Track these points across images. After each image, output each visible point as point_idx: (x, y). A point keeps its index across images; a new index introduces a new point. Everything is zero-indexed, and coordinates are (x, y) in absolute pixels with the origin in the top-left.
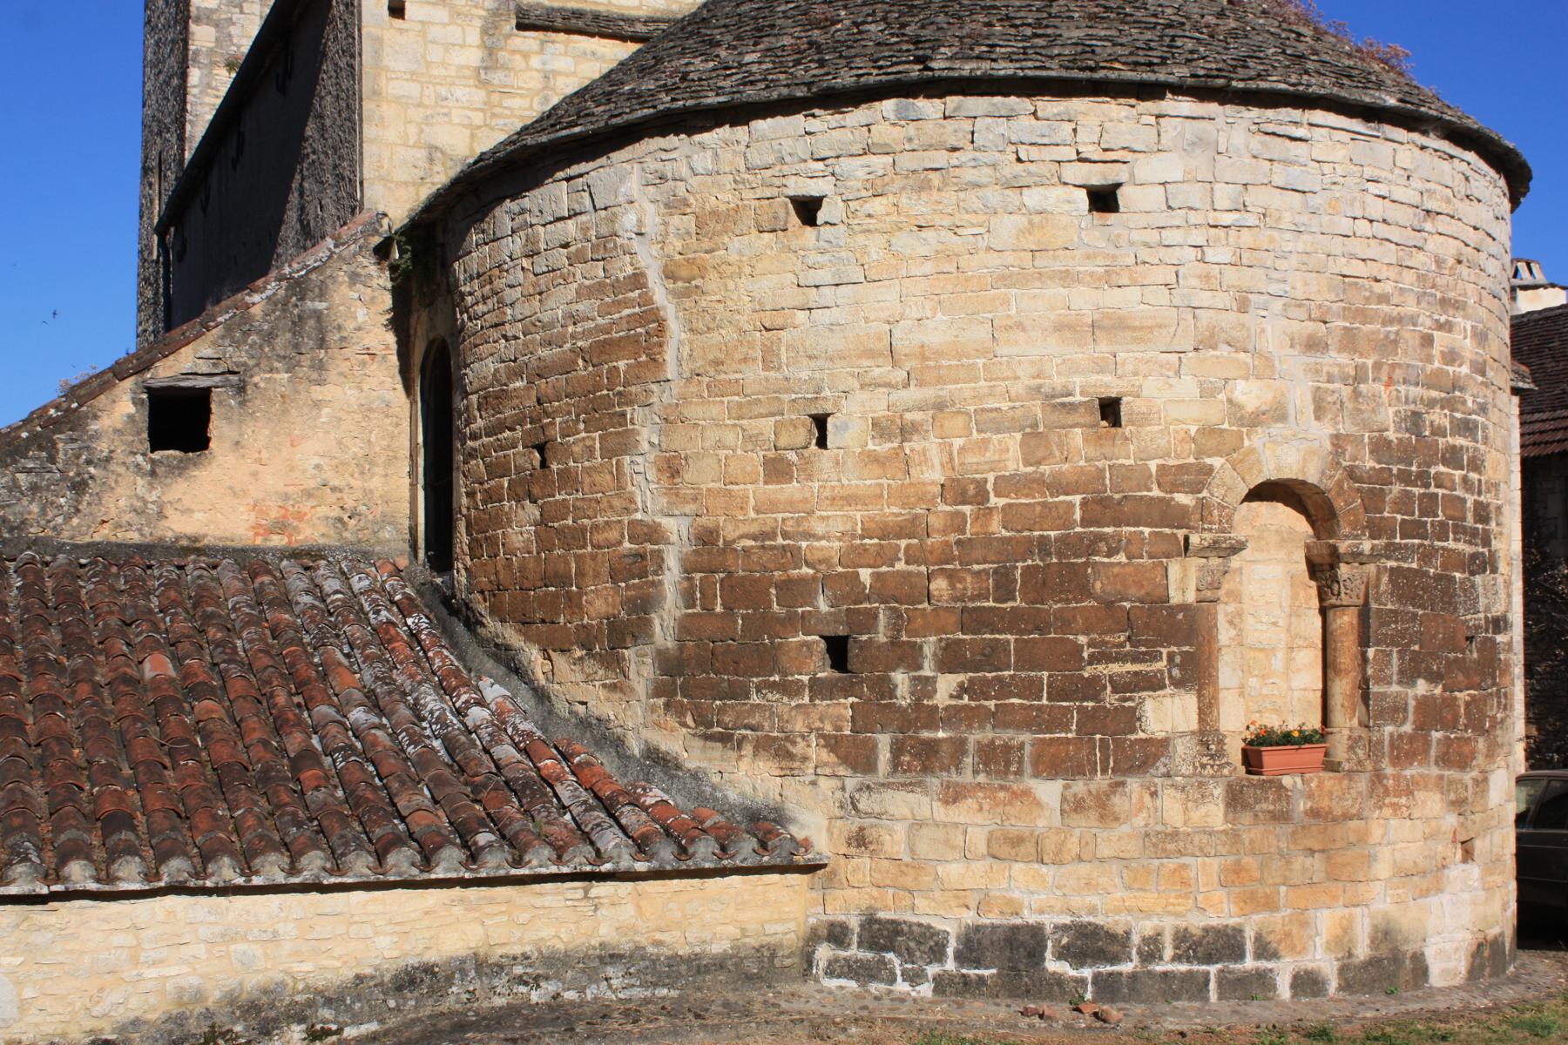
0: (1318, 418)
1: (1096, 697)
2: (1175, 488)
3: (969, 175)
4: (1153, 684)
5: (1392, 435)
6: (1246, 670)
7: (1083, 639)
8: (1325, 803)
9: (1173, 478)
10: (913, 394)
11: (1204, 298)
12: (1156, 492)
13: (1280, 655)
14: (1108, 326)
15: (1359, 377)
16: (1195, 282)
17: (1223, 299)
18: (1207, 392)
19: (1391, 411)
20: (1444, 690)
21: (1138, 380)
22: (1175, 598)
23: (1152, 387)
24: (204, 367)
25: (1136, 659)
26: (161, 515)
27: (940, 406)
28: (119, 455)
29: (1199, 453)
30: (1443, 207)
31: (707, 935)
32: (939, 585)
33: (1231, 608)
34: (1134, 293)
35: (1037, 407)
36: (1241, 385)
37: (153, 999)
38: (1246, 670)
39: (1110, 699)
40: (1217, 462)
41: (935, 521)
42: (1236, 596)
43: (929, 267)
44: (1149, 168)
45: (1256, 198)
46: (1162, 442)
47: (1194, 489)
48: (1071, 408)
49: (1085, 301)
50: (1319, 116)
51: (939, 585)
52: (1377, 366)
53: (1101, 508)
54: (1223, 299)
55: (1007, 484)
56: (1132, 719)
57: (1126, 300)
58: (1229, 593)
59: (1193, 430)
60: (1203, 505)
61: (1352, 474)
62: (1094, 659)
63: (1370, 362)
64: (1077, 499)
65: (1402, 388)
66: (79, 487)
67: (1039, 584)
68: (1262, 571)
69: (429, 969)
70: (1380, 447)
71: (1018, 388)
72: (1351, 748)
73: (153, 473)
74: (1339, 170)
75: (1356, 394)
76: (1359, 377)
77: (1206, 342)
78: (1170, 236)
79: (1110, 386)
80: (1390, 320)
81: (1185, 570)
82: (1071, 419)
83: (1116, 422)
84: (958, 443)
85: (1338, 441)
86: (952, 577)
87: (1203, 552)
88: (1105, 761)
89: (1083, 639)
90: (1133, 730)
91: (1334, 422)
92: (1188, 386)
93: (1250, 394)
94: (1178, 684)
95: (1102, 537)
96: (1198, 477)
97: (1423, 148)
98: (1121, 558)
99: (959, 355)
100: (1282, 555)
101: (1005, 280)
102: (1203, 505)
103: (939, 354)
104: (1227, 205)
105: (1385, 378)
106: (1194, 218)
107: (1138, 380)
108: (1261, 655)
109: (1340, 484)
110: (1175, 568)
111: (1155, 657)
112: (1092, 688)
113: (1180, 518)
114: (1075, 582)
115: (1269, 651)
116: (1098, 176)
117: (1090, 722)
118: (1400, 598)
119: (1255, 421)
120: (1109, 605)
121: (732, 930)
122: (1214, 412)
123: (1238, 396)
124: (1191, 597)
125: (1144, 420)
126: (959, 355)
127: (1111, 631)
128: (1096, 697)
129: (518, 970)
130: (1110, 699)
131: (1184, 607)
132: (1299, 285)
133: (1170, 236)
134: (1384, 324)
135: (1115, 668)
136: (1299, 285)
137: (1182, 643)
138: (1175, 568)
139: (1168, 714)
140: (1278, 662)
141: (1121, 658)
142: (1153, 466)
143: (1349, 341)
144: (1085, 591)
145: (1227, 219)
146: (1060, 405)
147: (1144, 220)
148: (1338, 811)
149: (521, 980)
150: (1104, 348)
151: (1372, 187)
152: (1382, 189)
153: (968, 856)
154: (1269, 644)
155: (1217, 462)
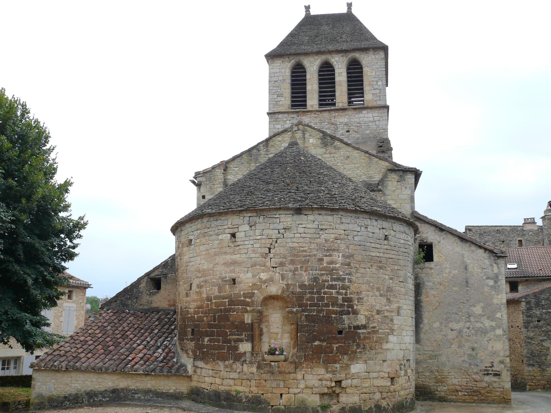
0: (282, 280)
1: (230, 343)
2: (245, 297)
3: (211, 233)
4: (241, 341)
5: (306, 283)
6: (270, 338)
7: (228, 331)
8: (283, 369)
9: (245, 295)
10: (202, 279)
11: (253, 255)
12: (242, 298)
13: (279, 335)
14: (234, 263)
15: (296, 269)
16: (251, 252)
17: (257, 255)
18: (254, 276)
19: (306, 278)
20: (327, 344)
21: (239, 274)
22: (246, 322)
23: (241, 275)
24: (159, 273)
25: (238, 335)
26: (151, 303)
27: (206, 281)
28: (144, 291)
29: (252, 290)
30: (328, 227)
31: (169, 388)
32: (205, 318)
33: (266, 324)
34: (238, 256)
35: (220, 281)
36: (262, 274)
37: (73, 390)
38: (270, 338)
39: (233, 343)
40: (256, 291)
41: (205, 305)
42: (268, 321)
43: (204, 253)
44: (242, 228)
45: (265, 232)
46: (244, 288)
47: (251, 298)
48: (226, 281)
49: (228, 258)
50: (281, 212)
51: (205, 318)
52: (301, 267)
53: (231, 303)
54: (257, 255)
55: (216, 297)
56: (237, 348)
57: (237, 257)
58: (266, 321)
59: (251, 285)
60: (252, 301)
61: (292, 293)
62: (230, 335)
63: (299, 266)
64: (227, 300)
65: (311, 272)
66: (137, 298)
67: (221, 318)
68: (274, 315)
69: (118, 390)
70: (302, 286)
71: (217, 277)
72: (292, 357)
73: (150, 295)
74: (289, 223)
75: (294, 274)
76: (296, 269)
77: (254, 265)
78: (246, 243)
79: (234, 275)
80: (306, 256)
81: (248, 316)
82: (226, 283)
83: (234, 283)
84: (208, 289)
85: (287, 285)
86: (207, 317)
87: (251, 312)
88: (232, 357)
89: (228, 331)
90: (237, 351)
91: (287, 281)
92: (250, 275)
93: (264, 276)
94: (247, 341)
95: (231, 308)
96: (252, 295)
97: (320, 214)
98: (235, 313)
99: (208, 271)
100: (280, 312)
101: (215, 255)
102: (252, 301)
103: (206, 271)
104: (258, 234)
105: (304, 270)
106: (251, 238)
107: (239, 274)
108: (274, 335)
109: (288, 295)
110: (246, 315)
111: (242, 335)
112: (229, 341)
113: (248, 304)
114: (227, 318)
115: (277, 334)
116: (232, 231)
117: (229, 348)
118: (308, 322)
119: (265, 282)
120: (233, 323)
121: (174, 388)
122: (255, 280)
123: (261, 277)
124: (250, 322)
125: (240, 283)
126: (208, 271)
127: (233, 329)
128: (230, 343)
129: (133, 391)
130: (233, 343)
131: (248, 324)
132: (278, 250)
133: (246, 243)
134: (304, 257)
135: (234, 337)
136: (278, 250)
137: (253, 333)
138: (246, 315)
139: (245, 347)
140: (279, 336)
141: (235, 335)
142: (242, 293)
143: (292, 262)
144: (228, 320)
145: (259, 237)
146: (223, 280)
147: (240, 240)
148: (287, 371)
149: (133, 393)
150: (232, 268)
151: (300, 226)
152: (304, 226)
153: (211, 376)
154: (277, 331)
155: (256, 291)
